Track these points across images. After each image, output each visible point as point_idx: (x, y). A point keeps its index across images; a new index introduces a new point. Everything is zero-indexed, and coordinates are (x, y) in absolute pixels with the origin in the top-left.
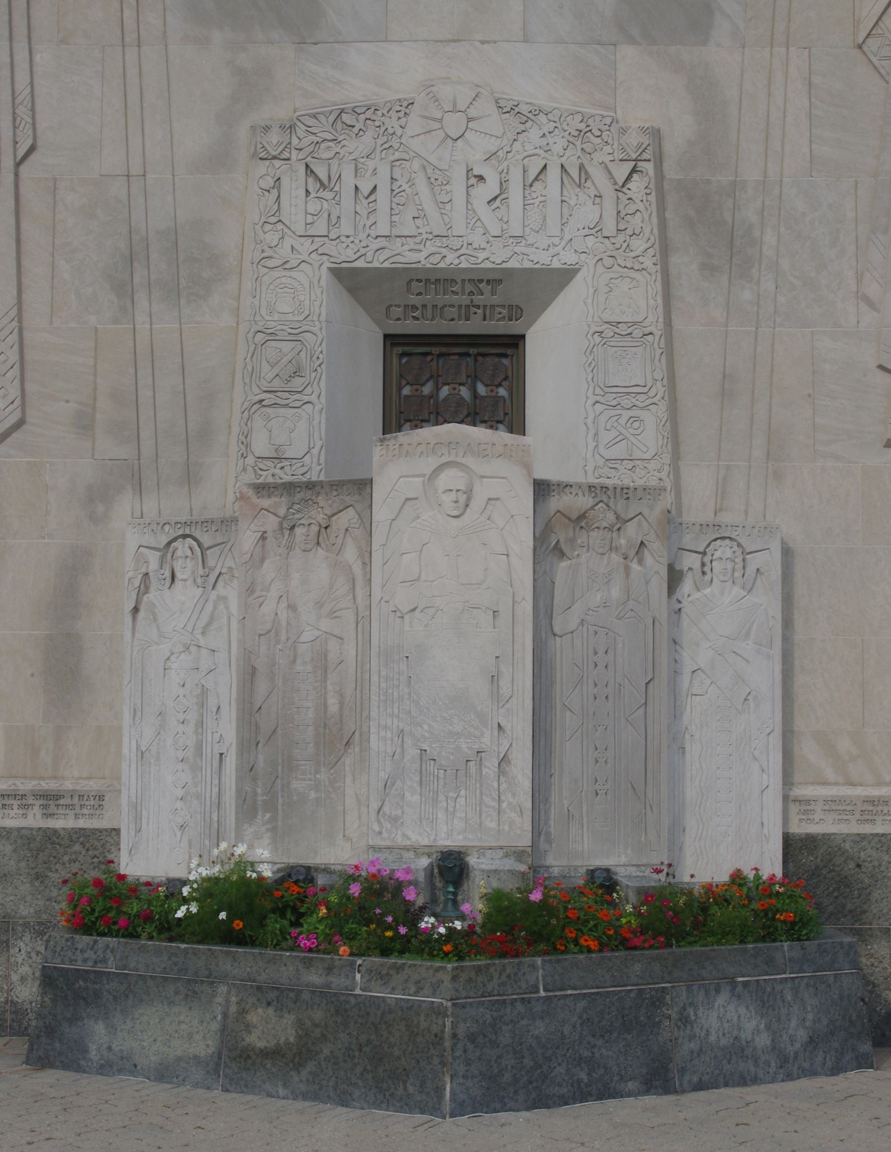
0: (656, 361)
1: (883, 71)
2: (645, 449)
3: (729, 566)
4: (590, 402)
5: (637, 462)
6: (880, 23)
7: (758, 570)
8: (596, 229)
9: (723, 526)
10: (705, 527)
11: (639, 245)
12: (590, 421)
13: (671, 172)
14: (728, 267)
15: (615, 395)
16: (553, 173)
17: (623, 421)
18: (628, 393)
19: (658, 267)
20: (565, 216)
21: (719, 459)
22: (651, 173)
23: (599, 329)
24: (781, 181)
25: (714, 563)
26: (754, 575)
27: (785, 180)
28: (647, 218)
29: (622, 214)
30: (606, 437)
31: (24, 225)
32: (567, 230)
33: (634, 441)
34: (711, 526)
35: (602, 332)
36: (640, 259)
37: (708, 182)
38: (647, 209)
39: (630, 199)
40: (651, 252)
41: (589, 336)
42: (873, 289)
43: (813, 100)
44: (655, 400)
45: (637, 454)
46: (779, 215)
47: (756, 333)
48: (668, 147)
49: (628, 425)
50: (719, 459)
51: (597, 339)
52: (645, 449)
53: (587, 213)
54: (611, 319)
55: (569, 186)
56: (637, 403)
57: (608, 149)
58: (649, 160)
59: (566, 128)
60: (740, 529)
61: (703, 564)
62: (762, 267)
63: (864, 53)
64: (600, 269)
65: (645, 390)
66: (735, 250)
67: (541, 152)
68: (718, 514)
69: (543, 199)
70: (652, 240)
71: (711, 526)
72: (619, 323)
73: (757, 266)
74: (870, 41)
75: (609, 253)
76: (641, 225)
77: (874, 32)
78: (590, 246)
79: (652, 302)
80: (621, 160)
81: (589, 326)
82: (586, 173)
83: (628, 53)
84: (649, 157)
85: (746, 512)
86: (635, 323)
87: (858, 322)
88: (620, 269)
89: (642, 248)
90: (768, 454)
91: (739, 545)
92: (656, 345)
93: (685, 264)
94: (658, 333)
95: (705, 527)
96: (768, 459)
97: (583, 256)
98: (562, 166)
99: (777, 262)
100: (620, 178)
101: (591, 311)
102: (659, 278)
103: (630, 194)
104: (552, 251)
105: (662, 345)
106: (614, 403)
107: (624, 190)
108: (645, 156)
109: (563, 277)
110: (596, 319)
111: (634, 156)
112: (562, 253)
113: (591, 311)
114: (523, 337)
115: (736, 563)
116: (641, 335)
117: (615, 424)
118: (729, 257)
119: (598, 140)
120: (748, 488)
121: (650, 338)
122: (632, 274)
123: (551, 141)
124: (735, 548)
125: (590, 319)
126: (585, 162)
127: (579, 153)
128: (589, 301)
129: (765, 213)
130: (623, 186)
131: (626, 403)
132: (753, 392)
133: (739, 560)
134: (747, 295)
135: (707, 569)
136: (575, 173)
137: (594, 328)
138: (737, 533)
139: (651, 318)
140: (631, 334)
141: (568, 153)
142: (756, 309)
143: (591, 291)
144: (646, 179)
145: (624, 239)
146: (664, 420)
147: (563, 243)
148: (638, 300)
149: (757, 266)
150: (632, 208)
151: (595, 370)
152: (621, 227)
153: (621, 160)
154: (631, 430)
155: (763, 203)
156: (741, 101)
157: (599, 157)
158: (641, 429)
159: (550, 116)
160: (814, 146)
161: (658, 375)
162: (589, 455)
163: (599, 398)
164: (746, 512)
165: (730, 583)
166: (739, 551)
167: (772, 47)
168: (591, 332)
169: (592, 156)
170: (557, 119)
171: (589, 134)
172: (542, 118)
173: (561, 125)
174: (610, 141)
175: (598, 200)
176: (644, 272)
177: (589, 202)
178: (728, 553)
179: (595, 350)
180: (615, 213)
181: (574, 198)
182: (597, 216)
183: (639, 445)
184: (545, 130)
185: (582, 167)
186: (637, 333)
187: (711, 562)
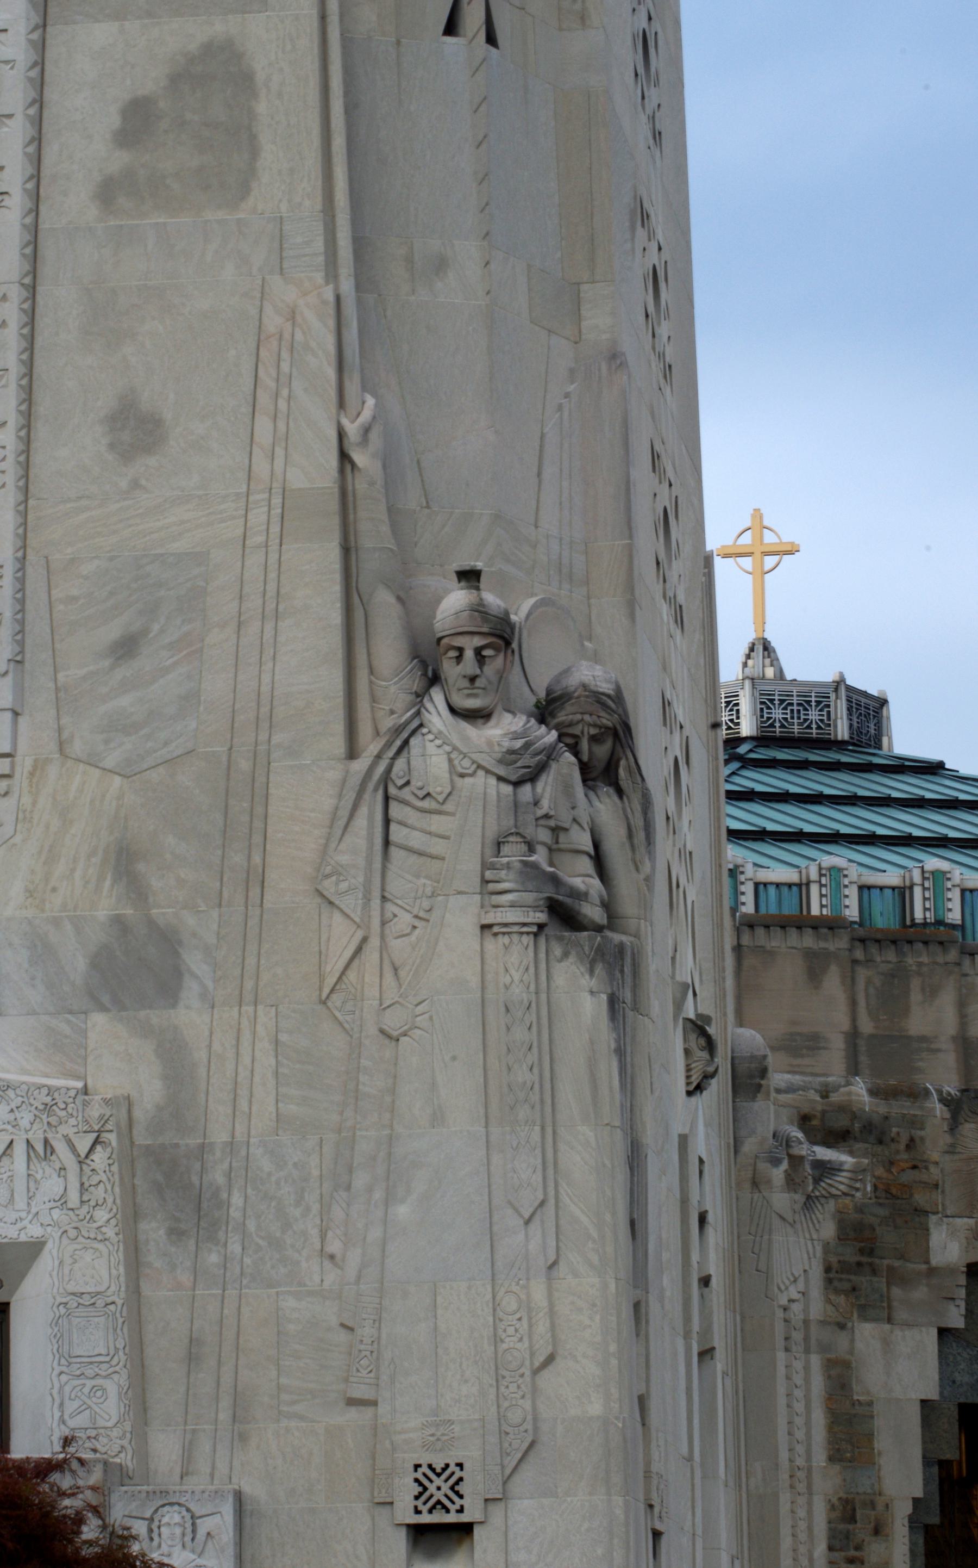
0: (119, 1331)
1: (346, 1026)
2: (107, 1417)
3: (178, 1531)
4: (56, 1372)
5: (102, 1431)
6: (344, 978)
7: (209, 1534)
8: (62, 1201)
9: (171, 1492)
10: (151, 1494)
11: (101, 1215)
12: (55, 1392)
13: (141, 1138)
14: (195, 1230)
15: (79, 1365)
16: (20, 1150)
17: (86, 1390)
18: (91, 1363)
19: (121, 1236)
20: (32, 1189)
21: (186, 1423)
22: (114, 1144)
23: (64, 1300)
24: (248, 1142)
25: (162, 1529)
26: (204, 1538)
27: (252, 1140)
28: (109, 1187)
29: (86, 1185)
30: (71, 1407)
31: (258, 390)
32: (33, 1204)
33: (98, 1410)
34: (158, 1493)
35: (66, 1304)
36: (104, 1230)
37: (177, 1146)
38: (109, 1180)
39: (93, 1170)
40: (113, 1222)
41: (55, 1308)
42: (334, 1246)
43: (280, 1058)
44: (117, 1368)
45: (101, 1423)
46: (247, 1176)
47: (223, 1296)
48: (138, 1114)
49: (92, 1394)
50: (186, 1423)
51: (62, 1310)
52: (107, 1417)
53: (52, 1185)
54: (75, 1290)
55: (35, 1160)
56: (100, 1372)
57: (73, 1121)
58: (111, 1131)
59: (32, 1101)
60: (188, 1495)
61: (150, 1531)
62: (230, 1229)
63: (328, 1008)
64: (65, 1241)
65: (107, 1359)
66: (202, 1213)
67: (9, 1127)
68: (185, 1478)
69: (10, 1174)
70: (115, 1210)
71: (158, 1493)
72: (83, 1294)
73: (224, 1228)
74: (334, 996)
75: (74, 1225)
76: (103, 1195)
77: (338, 987)
78: (55, 1217)
79: (114, 1272)
80: (85, 1132)
81: (54, 1298)
82: (52, 1147)
83: (99, 1019)
84: (111, 1128)
85: (212, 1476)
86: (98, 1293)
87: (322, 1281)
88: (84, 1240)
89: (105, 1218)
90: (234, 1416)
91: (188, 1510)
92: (118, 1315)
93: (153, 1231)
94: (119, 1302)
95: (151, 1494)
96: (234, 1421)
97: (49, 1229)
98: (28, 1141)
99: (244, 1224)
100: (83, 1150)
101: (56, 1283)
102: (121, 1248)
103: (93, 1165)
104: (19, 1225)
105: (124, 1314)
106: (78, 1373)
107: (88, 1161)
108: (108, 1127)
109: (35, 1248)
110: (61, 1290)
111: (96, 1128)
112: (29, 1226)
113: (56, 1283)
114: (8, 1304)
115: (185, 1528)
116: (103, 1305)
117: (79, 1394)
118: (196, 1221)
119: (63, 1113)
120: (215, 1451)
121: (112, 1307)
122: (96, 1245)
123: (18, 1115)
124: (184, 1513)
125: (55, 1290)
126: (50, 1136)
127: (46, 1127)
128: (55, 1273)
129: (233, 1174)
130: (87, 1157)
131: (89, 1372)
132: (220, 1356)
133: (188, 1525)
134: (214, 1258)
135: (155, 1536)
136: (40, 1148)
137: (59, 1300)
138: (185, 1499)
139: (113, 1288)
140: (94, 1304)
141: (35, 1127)
142: (222, 1271)
143: (57, 1263)
144: (109, 1150)
145: (87, 1210)
146: (125, 1388)
147: (30, 1217)
148: (99, 1270)
149: (224, 1228)
150: (95, 1179)
151: (60, 1342)
152: (85, 1198)
153: (85, 1132)
154: (94, 1399)
155: (231, 1163)
156: (209, 1062)
157: (63, 1130)
158: (104, 1397)
159: (18, 1091)
160: (280, 1105)
161: (120, 1344)
162: (55, 1425)
163: (64, 1369)
164: (212, 1476)
165: (180, 1546)
166: (188, 1516)
167: (240, 1006)
168: (57, 1304)
169: (58, 1129)
170: (24, 1094)
171: (54, 1107)
172: (11, 1093)
173: (28, 1099)
174: (75, 1114)
175: (63, 1173)
176: (107, 1242)
177: (55, 1175)
178: (177, 1518)
179: (60, 1321)
180: (78, 1185)
181: (40, 1171)
182: (62, 1189)
183: (102, 1413)
184: (13, 1105)
185: (46, 1141)
186: (100, 1303)
187: (159, 1527)
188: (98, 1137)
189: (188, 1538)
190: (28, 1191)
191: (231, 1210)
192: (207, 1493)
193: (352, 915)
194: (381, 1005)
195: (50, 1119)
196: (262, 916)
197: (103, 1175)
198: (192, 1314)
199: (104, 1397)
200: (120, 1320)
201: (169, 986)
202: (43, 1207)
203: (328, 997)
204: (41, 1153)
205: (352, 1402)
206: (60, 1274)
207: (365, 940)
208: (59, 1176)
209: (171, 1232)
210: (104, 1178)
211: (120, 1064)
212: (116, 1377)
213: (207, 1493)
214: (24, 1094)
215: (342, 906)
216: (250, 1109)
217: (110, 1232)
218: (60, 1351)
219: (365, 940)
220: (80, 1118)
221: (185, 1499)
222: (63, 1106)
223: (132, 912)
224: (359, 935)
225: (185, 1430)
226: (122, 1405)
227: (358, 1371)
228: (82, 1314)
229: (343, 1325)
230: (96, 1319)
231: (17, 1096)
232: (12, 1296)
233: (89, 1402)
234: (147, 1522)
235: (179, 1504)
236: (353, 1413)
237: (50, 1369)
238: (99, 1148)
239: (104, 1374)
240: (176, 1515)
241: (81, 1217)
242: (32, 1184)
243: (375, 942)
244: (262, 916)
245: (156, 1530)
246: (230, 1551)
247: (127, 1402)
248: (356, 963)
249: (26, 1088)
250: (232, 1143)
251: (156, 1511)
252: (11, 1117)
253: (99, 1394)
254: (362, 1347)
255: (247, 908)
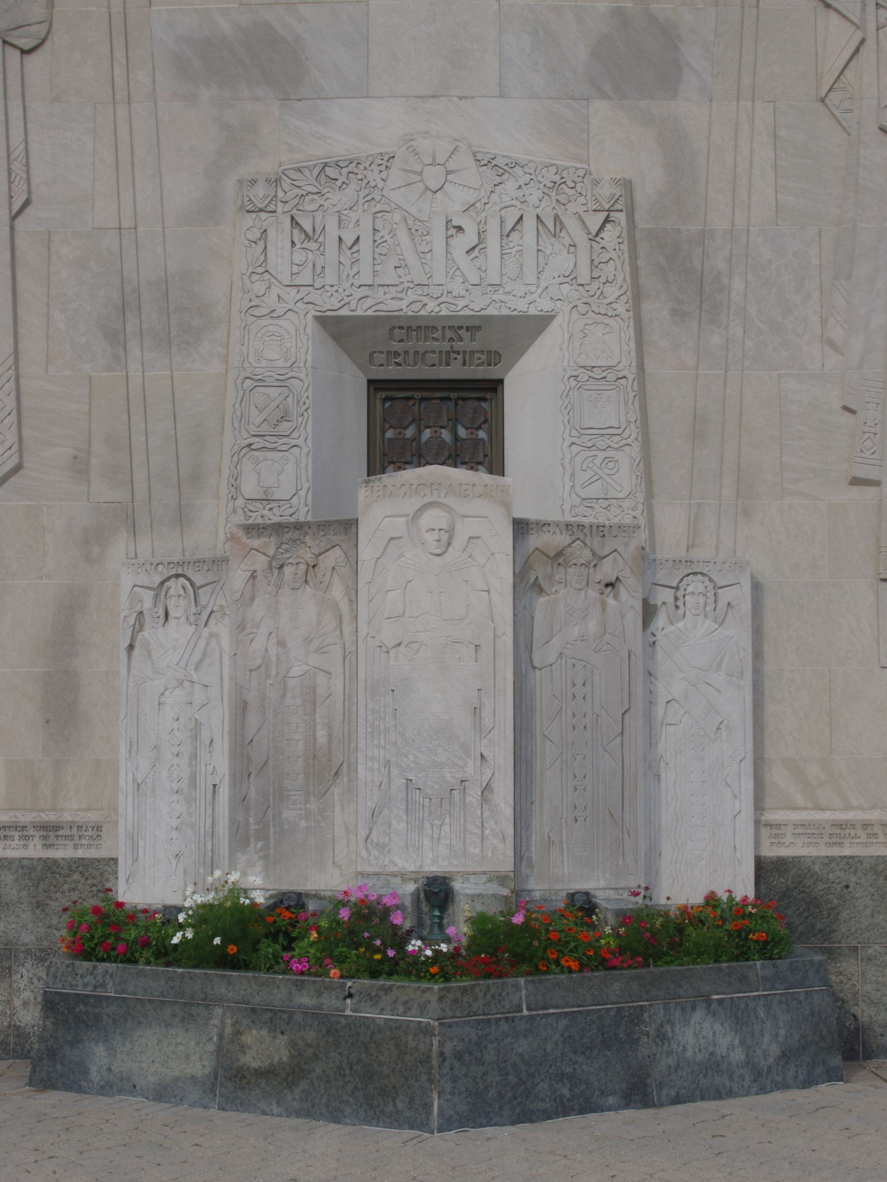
1: (844, 123)
2: (619, 489)
3: (702, 600)
4: (567, 443)
6: (842, 77)
7: (729, 604)
8: (571, 277)
9: (696, 562)
10: (677, 562)
11: (612, 292)
13: (642, 221)
14: (698, 312)
15: (590, 437)
16: (530, 224)
17: (598, 461)
18: (603, 435)
19: (631, 313)
23: (575, 373)
24: (748, 230)
26: (725, 608)
27: (751, 229)
28: (619, 266)
29: (596, 262)
30: (582, 477)
32: (543, 278)
33: (610, 481)
37: (679, 231)
40: (624, 299)
42: (837, 333)
43: (778, 152)
44: (629, 441)
45: (612, 494)
47: (726, 376)
49: (604, 465)
51: (573, 382)
52: (619, 489)
53: (562, 262)
55: (544, 236)
56: (612, 444)
57: (582, 200)
58: (621, 211)
61: (676, 599)
62: (731, 312)
64: (575, 315)
65: (619, 431)
67: (517, 203)
69: (519, 248)
70: (625, 287)
72: (594, 367)
76: (614, 273)
78: (565, 293)
79: (625, 347)
81: (565, 370)
82: (561, 223)
83: (600, 108)
86: (609, 367)
87: (823, 365)
89: (615, 295)
90: (738, 492)
91: (711, 580)
92: (629, 389)
93: (657, 311)
94: (631, 377)
95: (677, 562)
96: (737, 497)
98: (538, 217)
101: (567, 355)
102: (632, 324)
104: (529, 298)
106: (590, 444)
107: (598, 239)
108: (618, 206)
110: (572, 363)
111: (607, 207)
112: (538, 300)
113: (567, 355)
116: (615, 379)
117: (591, 465)
119: (573, 192)
120: (719, 526)
121: (623, 381)
123: (527, 193)
124: (707, 583)
125: (565, 363)
126: (560, 213)
127: (554, 204)
128: (565, 346)
129: (733, 260)
130: (596, 235)
132: (723, 433)
133: (711, 594)
134: (716, 340)
136: (550, 224)
138: (708, 569)
143: (567, 337)
144: (619, 228)
145: (597, 287)
146: (638, 460)
148: (612, 345)
150: (605, 257)
152: (595, 275)
154: (606, 470)
157: (572, 208)
158: (616, 469)
159: (526, 169)
160: (779, 196)
162: (566, 495)
163: (575, 440)
164: (717, 549)
165: (702, 616)
167: (738, 101)
168: (567, 376)
171: (563, 186)
172: (518, 171)
174: (584, 192)
175: (572, 249)
178: (701, 588)
179: (571, 393)
181: (550, 247)
182: (572, 264)
184: (521, 182)
185: (556, 218)
186: (611, 377)
187: (684, 596)
188: (608, 216)
189: (709, 608)
190: (538, 266)
191: (733, 295)
192: (728, 564)
193: (851, 17)
194: (879, 104)
195: (559, 197)
196: (758, 16)
197: (613, 252)
198: (696, 392)
199: (616, 469)
200: (632, 394)
201: (668, 77)
202: (553, 281)
203: (826, 95)
204: (552, 229)
205: (856, 481)
206: (570, 347)
207: (863, 41)
208: (569, 253)
209: (674, 312)
210: (614, 255)
211: (619, 148)
212: (627, 448)
213: (728, 564)
214: (532, 172)
215: (840, 8)
216: (749, 198)
217: (621, 308)
218: (571, 422)
219: (863, 41)
220: (589, 197)
221: (708, 569)
222: (572, 185)
223: (632, 5)
224: (858, 36)
225: (690, 504)
226: (634, 477)
227: (862, 451)
228: (593, 387)
229: (845, 408)
230: (608, 393)
231: (525, 173)
232: (507, 372)
233: (601, 474)
234: (674, 591)
235: (702, 574)
236: (856, 491)
237: (561, 440)
238: (608, 226)
239: (616, 446)
240: (700, 584)
241: (591, 293)
242: (541, 259)
243: (870, 44)
244: (758, 16)
245: (681, 598)
246: (749, 621)
247: (639, 474)
248: (854, 62)
249: (535, 166)
250: (732, 230)
251: (681, 580)
252: (520, 193)
253: (611, 465)
254: (866, 429)
255: (743, 7)
